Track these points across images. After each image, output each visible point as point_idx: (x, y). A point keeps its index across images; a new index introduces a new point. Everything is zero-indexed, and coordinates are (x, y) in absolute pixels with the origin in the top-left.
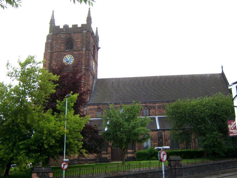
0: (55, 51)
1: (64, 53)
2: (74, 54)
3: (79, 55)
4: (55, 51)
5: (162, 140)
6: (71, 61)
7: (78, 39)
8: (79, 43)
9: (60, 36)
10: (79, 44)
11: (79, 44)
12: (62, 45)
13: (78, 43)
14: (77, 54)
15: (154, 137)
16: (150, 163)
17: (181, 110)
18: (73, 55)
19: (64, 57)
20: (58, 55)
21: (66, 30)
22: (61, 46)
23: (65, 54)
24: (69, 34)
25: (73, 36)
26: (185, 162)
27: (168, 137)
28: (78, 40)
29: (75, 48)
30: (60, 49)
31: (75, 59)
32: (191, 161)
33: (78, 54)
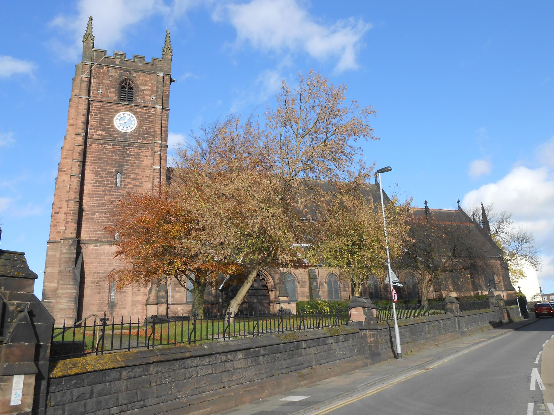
0: (96, 99)
1: (115, 107)
2: (137, 112)
3: (144, 137)
4: (96, 99)
5: (317, 284)
6: (132, 126)
7: (147, 85)
8: (149, 93)
9: (108, 71)
10: (147, 95)
11: (147, 95)
12: (112, 90)
13: (146, 92)
14: (143, 113)
15: (302, 278)
16: (104, 325)
17: (416, 210)
18: (135, 113)
19: (115, 115)
20: (102, 108)
21: (120, 62)
22: (110, 92)
23: (118, 110)
24: (126, 71)
25: (135, 77)
26: (292, 325)
27: (324, 280)
28: (146, 88)
29: (139, 100)
30: (108, 97)
31: (139, 123)
32: (292, 323)
33: (146, 113)
